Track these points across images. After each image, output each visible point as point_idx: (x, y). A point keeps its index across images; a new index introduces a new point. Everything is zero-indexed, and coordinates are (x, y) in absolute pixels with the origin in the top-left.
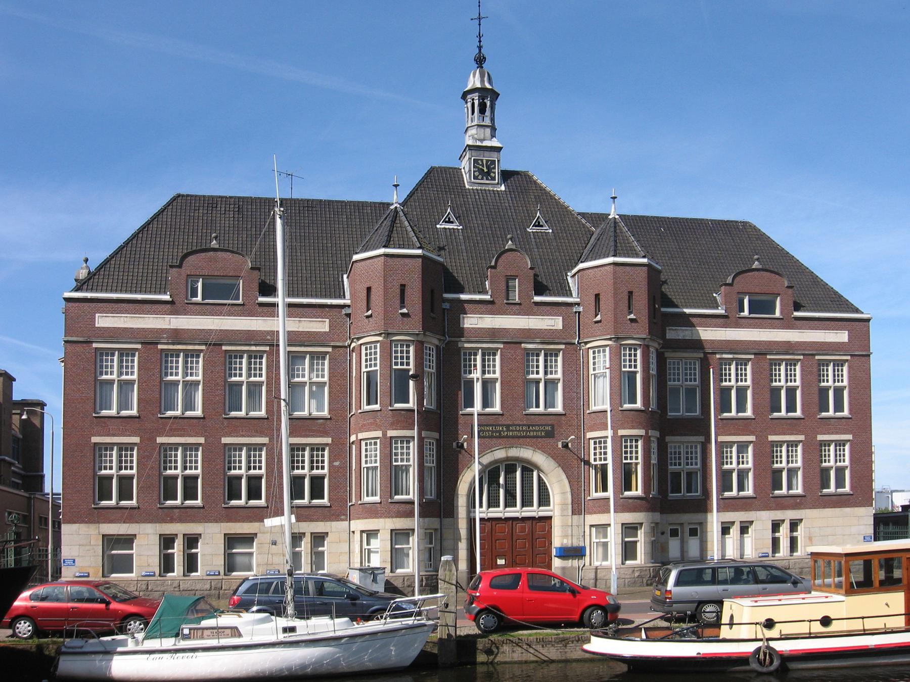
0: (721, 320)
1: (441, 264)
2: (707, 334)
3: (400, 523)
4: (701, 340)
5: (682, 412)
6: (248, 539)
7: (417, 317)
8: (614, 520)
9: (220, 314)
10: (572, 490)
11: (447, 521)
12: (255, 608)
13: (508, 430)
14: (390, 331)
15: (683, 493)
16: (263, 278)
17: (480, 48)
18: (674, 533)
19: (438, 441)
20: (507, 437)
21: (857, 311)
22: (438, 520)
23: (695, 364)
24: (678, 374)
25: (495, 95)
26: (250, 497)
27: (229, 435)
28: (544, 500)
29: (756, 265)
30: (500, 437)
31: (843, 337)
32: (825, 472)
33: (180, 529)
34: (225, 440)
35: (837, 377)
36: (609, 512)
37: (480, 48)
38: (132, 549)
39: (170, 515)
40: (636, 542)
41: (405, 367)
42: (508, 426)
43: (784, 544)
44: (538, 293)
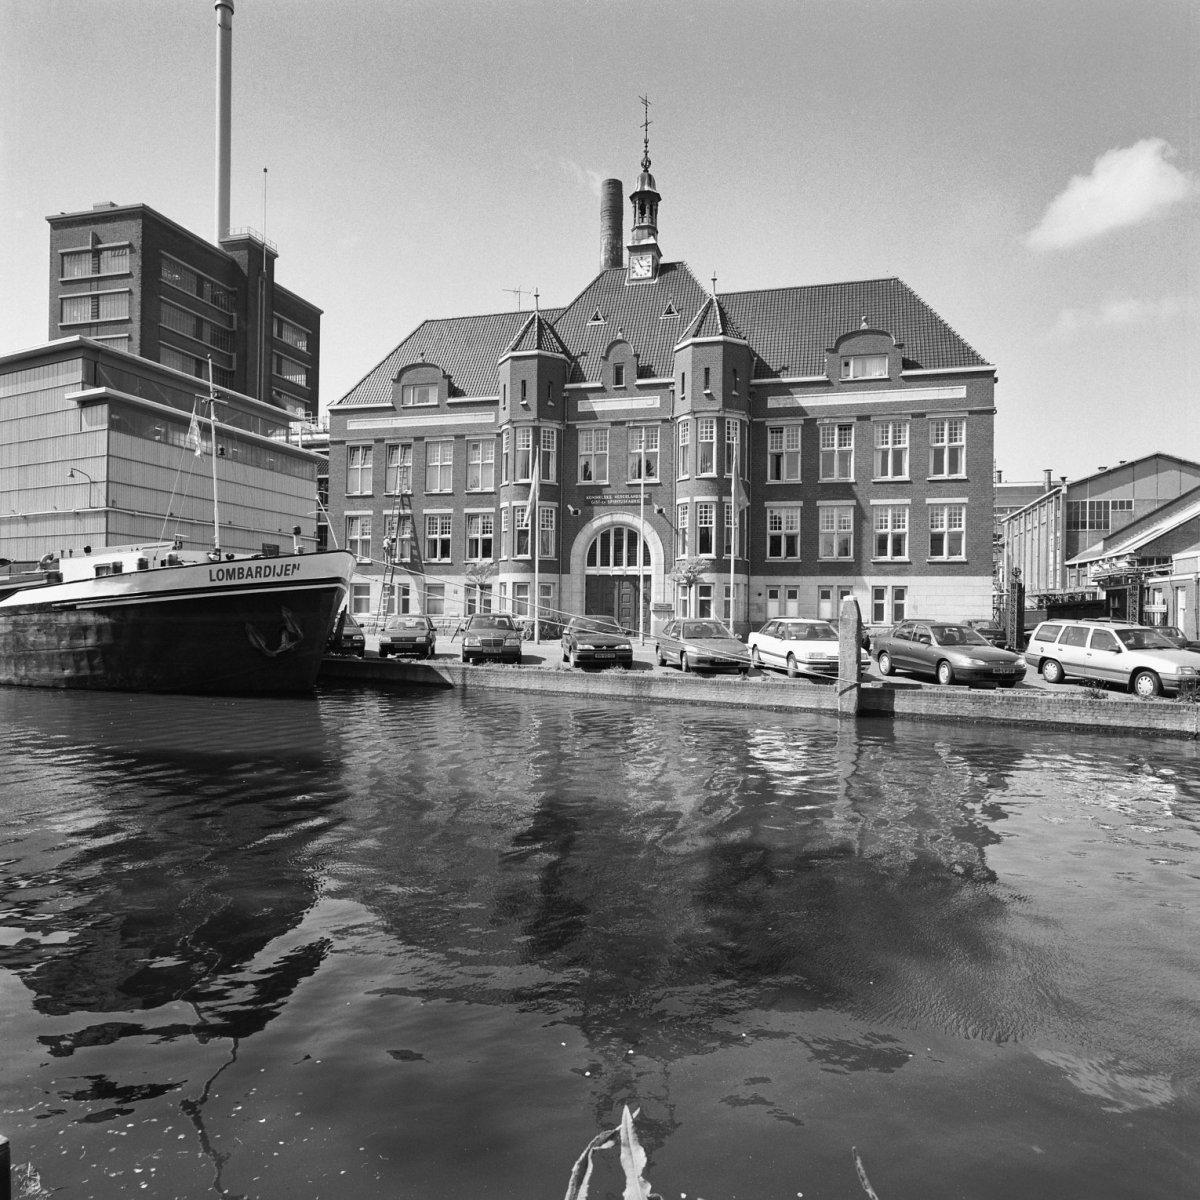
0: (887, 383)
1: (746, 347)
2: (806, 401)
3: (520, 578)
4: (802, 408)
5: (836, 478)
6: (440, 588)
7: (719, 396)
8: (509, 578)
9: (429, 413)
10: (664, 551)
11: (564, 576)
12: (605, 648)
13: (614, 499)
14: (695, 409)
15: (782, 557)
16: (907, 356)
17: (646, 152)
18: (774, 595)
19: (557, 509)
20: (612, 505)
21: (983, 363)
22: (746, 576)
23: (797, 431)
24: (591, 444)
25: (656, 198)
26: (951, 553)
27: (427, 507)
28: (647, 562)
29: (864, 326)
30: (607, 505)
31: (960, 392)
32: (937, 540)
33: (890, 581)
34: (929, 501)
35: (601, 445)
36: (729, 572)
37: (646, 152)
38: (709, 596)
39: (882, 569)
40: (709, 602)
41: (708, 440)
42: (613, 495)
43: (888, 611)
44: (640, 376)
